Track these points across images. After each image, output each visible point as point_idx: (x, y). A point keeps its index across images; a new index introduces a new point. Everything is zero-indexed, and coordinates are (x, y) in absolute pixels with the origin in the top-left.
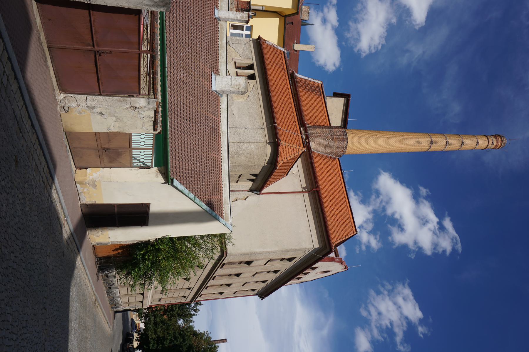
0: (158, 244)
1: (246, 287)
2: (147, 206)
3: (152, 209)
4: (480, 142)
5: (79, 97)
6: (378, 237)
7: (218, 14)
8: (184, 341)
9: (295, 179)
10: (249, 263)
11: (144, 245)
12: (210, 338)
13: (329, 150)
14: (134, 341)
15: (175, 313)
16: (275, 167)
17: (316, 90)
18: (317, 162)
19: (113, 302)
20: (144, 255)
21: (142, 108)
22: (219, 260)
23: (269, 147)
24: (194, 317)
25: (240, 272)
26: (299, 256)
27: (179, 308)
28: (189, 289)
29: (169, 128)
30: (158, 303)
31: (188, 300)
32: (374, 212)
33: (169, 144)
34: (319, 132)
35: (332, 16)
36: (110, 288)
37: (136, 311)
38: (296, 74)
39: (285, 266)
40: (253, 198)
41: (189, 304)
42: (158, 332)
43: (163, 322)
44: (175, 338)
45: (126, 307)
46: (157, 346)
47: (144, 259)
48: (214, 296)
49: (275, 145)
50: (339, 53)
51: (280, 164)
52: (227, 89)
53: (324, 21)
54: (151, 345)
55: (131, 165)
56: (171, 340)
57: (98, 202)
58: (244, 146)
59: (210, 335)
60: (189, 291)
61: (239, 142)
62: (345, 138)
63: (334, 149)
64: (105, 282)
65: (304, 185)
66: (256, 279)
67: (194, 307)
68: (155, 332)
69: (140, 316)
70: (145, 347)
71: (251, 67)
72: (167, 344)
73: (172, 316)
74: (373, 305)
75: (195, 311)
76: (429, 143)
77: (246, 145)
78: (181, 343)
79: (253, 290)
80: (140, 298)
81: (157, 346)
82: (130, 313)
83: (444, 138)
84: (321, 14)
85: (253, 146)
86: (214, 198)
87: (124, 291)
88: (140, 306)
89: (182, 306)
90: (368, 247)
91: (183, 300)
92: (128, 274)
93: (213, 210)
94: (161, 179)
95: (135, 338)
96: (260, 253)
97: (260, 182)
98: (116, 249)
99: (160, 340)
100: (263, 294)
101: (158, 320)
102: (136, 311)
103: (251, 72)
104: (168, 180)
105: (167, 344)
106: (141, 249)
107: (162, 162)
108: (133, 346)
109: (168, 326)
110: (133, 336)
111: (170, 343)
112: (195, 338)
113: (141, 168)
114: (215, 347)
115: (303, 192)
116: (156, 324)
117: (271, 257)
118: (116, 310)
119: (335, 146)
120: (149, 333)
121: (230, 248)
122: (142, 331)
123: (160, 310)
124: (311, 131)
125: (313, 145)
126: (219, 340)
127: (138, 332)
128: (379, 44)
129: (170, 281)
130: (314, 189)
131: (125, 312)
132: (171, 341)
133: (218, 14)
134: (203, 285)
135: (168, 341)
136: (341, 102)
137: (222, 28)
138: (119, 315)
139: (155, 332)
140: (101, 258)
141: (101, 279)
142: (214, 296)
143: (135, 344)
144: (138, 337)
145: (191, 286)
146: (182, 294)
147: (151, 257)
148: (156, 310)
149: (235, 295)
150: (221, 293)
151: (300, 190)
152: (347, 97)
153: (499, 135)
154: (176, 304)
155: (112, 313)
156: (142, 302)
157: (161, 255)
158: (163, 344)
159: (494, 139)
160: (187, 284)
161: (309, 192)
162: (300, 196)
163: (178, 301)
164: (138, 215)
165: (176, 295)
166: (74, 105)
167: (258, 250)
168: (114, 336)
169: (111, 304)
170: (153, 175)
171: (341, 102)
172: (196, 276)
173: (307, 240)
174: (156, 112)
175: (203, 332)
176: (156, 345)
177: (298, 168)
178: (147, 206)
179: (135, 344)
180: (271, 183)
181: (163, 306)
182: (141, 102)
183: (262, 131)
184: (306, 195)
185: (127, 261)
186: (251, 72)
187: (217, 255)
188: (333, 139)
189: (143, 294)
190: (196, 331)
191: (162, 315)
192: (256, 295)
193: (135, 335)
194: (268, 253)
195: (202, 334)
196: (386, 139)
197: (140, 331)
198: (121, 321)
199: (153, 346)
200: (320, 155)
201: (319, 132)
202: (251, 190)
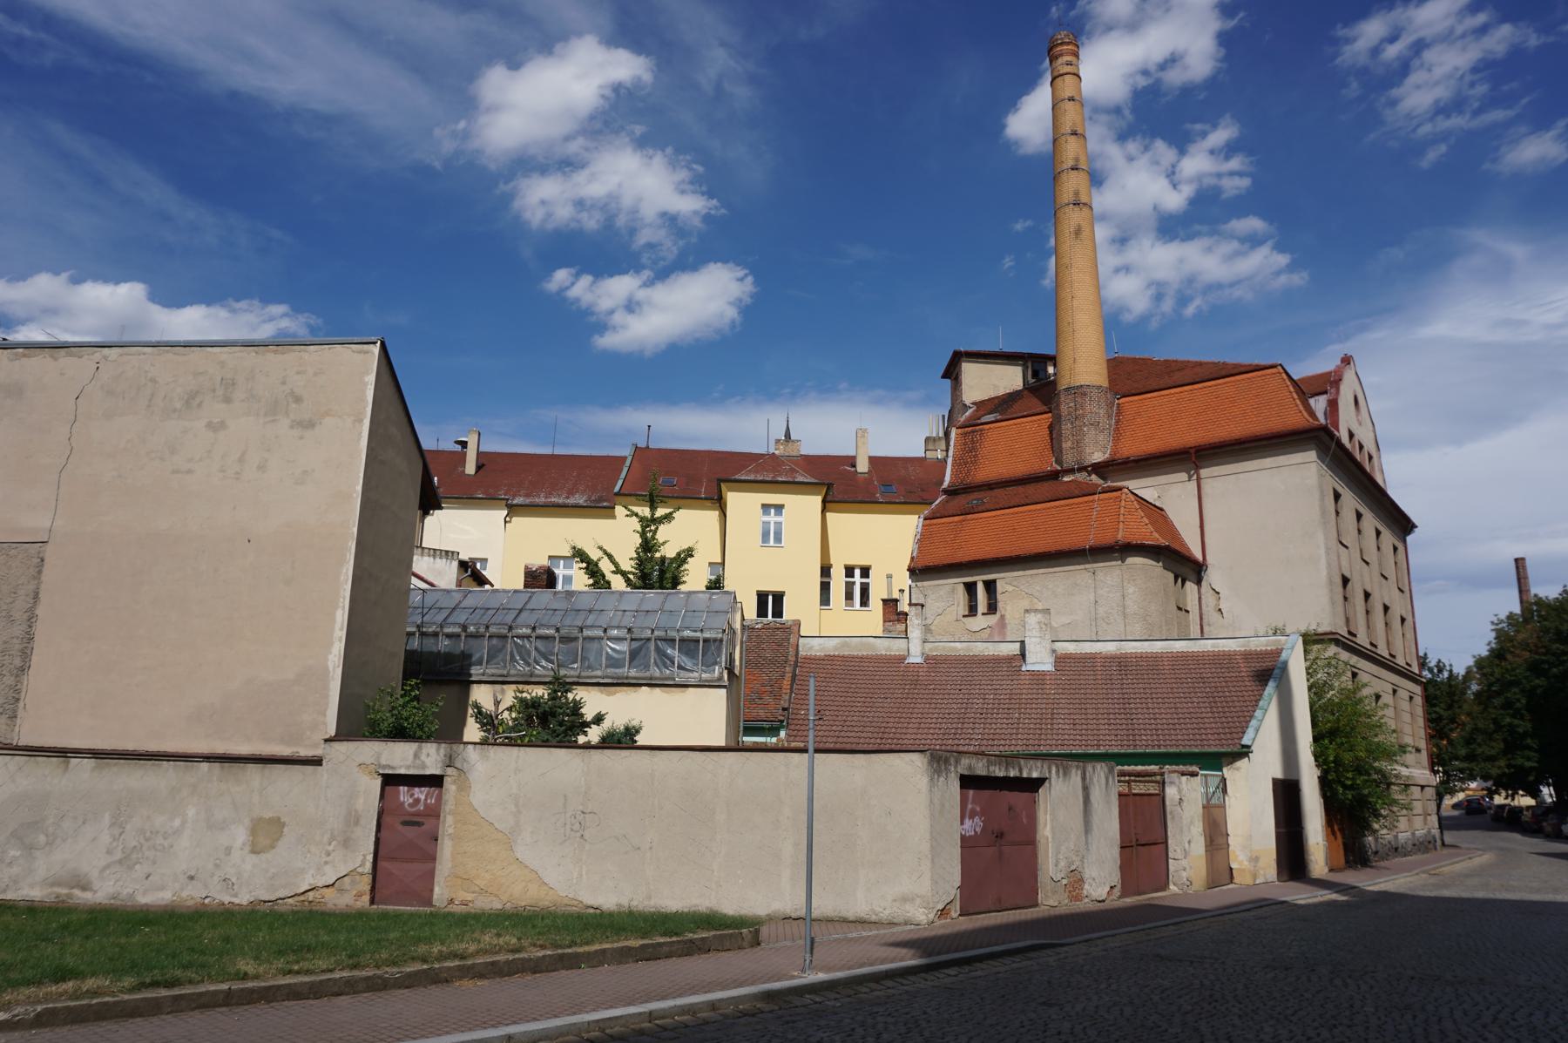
0: (1326, 762)
1: (1390, 571)
2: (1276, 782)
3: (1279, 775)
4: (1068, 94)
5: (1171, 868)
6: (1198, 127)
7: (915, 658)
8: (1516, 683)
9: (1171, 494)
10: (1345, 581)
11: (1325, 783)
12: (1511, 616)
13: (1104, 422)
14: (1516, 803)
15: (1445, 714)
16: (1167, 548)
17: (973, 442)
18: (1133, 447)
19: (1424, 845)
20: (1345, 787)
21: (1180, 791)
22: (1337, 642)
23: (1130, 560)
24: (1455, 671)
25: (1362, 596)
26: (1332, 482)
27: (1434, 705)
28: (1395, 691)
29: (1163, 750)
30: (1424, 753)
31: (1418, 689)
32: (1122, 137)
33: (1188, 750)
34: (1069, 444)
35: (621, 286)
36: (1396, 850)
37: (1440, 797)
38: (946, 484)
39: (1350, 501)
40: (1213, 576)
41: (1426, 686)
42: (1493, 752)
43: (1469, 741)
44: (1508, 705)
45: (1434, 819)
46: (1529, 748)
47: (1351, 788)
48: (1409, 636)
49: (1124, 550)
50: (712, 266)
51: (1163, 542)
52: (1047, 644)
53: (631, 306)
54: (1528, 764)
55: (1223, 806)
56: (1513, 716)
57: (1274, 856)
58: (1132, 607)
59: (1503, 616)
60: (1401, 692)
61: (1125, 616)
62: (1078, 391)
63: (1102, 412)
64: (1386, 857)
65: (1184, 476)
66: (1372, 555)
67: (1430, 670)
68: (1492, 759)
69: (1452, 792)
70: (1531, 778)
71: (970, 588)
72: (1524, 726)
73: (1453, 721)
74: (1414, 130)
75: (1440, 671)
76: (1076, 208)
77: (1128, 602)
78: (1523, 691)
79: (1395, 549)
80: (1416, 791)
81: (1529, 748)
82: (1444, 813)
83: (1064, 176)
84: (618, 318)
85: (1131, 591)
86: (1245, 670)
87: (1403, 823)
88: (1430, 792)
89: (1429, 700)
90: (1229, 150)
91: (1418, 700)
92: (1377, 815)
93: (1268, 671)
94: (1242, 763)
95: (1508, 801)
96: (1329, 565)
97: (1185, 566)
98: (1333, 833)
99: (1513, 745)
100: (1402, 524)
101: (1463, 752)
102: (1440, 797)
103: (980, 588)
104: (1244, 752)
105: (1524, 726)
106: (1335, 793)
107: (1217, 760)
108: (1528, 808)
109: (1476, 729)
110: (1502, 807)
111: (1522, 718)
112: (1509, 657)
113: (1225, 791)
114: (1536, 603)
115: (1199, 480)
116: (1471, 757)
117: (1335, 542)
118: (1439, 843)
119: (1096, 409)
120: (1495, 772)
121: (1325, 628)
122: (1489, 784)
123: (1437, 746)
124: (1069, 460)
125: (1098, 457)
126: (1519, 579)
127: (1491, 793)
128: (691, 169)
129: (1393, 739)
130: (1191, 458)
131: (1444, 824)
132: (1516, 714)
133: (915, 658)
134: (1388, 665)
135: (1516, 722)
136: (969, 370)
137: (936, 649)
138: (1449, 837)
139: (1492, 759)
140: (1347, 862)
141: (1382, 864)
142: (1409, 636)
143: (1527, 801)
144: (1504, 794)
145: (1389, 688)
146: (1405, 705)
147: (1350, 775)
148: (1438, 756)
149: (1406, 589)
150: (1403, 620)
151: (1194, 484)
152: (957, 358)
153: (1050, 50)
154: (1427, 713)
155: (1446, 851)
156: (1423, 787)
157: (1347, 757)
158: (1525, 734)
159: (1060, 61)
160: (1387, 698)
161: (1197, 468)
162: (1207, 486)
163: (1419, 711)
164: (1287, 794)
165: (1407, 717)
166: (1184, 874)
167: (1324, 573)
168: (1502, 849)
169: (1427, 850)
170: (1236, 775)
171: (969, 370)
172: (1375, 681)
173: (1302, 472)
174: (1183, 774)
175: (1493, 634)
176: (1527, 753)
177: (1148, 488)
178: (1276, 782)
179: (1527, 801)
180: (1183, 544)
181: (1430, 738)
182: (1171, 792)
183: (1100, 575)
184: (1204, 472)
185: (1353, 812)
186: (980, 588)
187: (1332, 650)
188: (1083, 416)
189: (1407, 786)
190: (1492, 651)
191: (1450, 742)
192: (1405, 542)
193: (1499, 800)
194: (1328, 549)
195: (1500, 635)
196: (1075, 303)
197: (1488, 789)
198: (1463, 833)
199: (1529, 759)
200: (1116, 440)
201: (1069, 444)
202: (1199, 582)
